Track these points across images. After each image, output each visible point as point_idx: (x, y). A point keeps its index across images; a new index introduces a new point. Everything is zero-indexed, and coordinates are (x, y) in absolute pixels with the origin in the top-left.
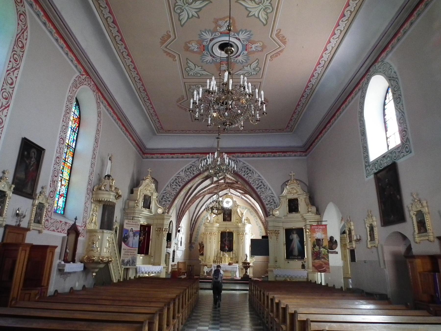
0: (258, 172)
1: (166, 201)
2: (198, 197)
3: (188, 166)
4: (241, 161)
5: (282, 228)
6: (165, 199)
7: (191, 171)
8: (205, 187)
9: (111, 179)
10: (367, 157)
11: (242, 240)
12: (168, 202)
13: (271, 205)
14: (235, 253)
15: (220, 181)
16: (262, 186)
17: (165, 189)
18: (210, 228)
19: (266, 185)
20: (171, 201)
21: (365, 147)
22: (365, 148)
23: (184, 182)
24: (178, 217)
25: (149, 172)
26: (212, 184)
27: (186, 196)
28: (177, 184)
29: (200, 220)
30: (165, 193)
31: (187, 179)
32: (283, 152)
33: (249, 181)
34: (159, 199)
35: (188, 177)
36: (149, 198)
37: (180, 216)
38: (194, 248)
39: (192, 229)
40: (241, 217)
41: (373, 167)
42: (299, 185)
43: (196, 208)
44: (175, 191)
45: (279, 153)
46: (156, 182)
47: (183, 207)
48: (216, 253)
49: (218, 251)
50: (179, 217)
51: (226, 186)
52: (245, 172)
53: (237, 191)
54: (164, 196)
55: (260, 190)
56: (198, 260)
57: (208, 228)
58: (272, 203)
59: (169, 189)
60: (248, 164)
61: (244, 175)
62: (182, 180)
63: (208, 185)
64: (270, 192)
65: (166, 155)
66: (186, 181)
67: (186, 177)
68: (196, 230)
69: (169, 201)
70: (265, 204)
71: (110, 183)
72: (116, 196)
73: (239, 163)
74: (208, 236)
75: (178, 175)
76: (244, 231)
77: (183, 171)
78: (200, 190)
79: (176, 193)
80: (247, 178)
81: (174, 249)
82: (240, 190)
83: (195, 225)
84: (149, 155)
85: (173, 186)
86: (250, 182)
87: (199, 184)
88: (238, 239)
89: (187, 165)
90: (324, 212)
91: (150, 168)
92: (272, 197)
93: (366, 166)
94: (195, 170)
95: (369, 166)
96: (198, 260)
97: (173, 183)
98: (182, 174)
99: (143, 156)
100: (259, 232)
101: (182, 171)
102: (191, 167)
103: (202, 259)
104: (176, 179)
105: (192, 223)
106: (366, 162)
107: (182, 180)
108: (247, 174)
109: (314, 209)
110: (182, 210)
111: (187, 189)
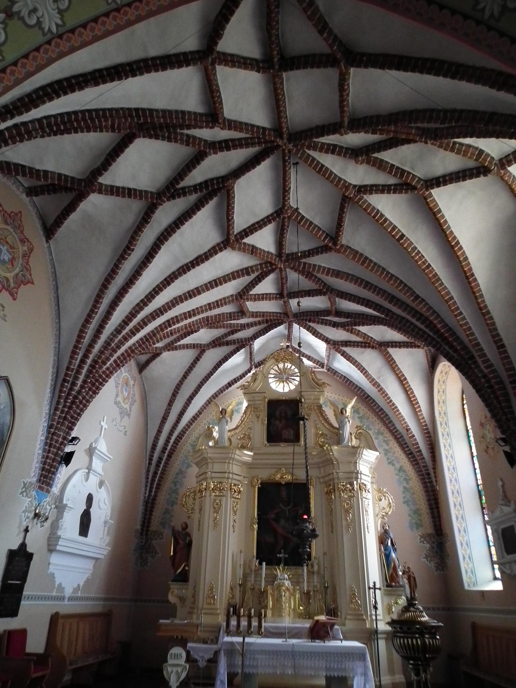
8: (196, 259)
11: (347, 511)
14: (318, 573)
18: (217, 467)
27: (105, 286)
29: (185, 447)
38: (156, 553)
39: (153, 480)
40: (336, 425)
43: (171, 403)
48: (240, 573)
49: (247, 565)
57: (210, 465)
63: (206, 249)
68: (167, 485)
74: (208, 498)
76: (355, 474)
78: (173, 273)
83: (165, 466)
87: (166, 230)
88: (331, 512)
100: (402, 489)
103: (182, 599)
105: (154, 462)
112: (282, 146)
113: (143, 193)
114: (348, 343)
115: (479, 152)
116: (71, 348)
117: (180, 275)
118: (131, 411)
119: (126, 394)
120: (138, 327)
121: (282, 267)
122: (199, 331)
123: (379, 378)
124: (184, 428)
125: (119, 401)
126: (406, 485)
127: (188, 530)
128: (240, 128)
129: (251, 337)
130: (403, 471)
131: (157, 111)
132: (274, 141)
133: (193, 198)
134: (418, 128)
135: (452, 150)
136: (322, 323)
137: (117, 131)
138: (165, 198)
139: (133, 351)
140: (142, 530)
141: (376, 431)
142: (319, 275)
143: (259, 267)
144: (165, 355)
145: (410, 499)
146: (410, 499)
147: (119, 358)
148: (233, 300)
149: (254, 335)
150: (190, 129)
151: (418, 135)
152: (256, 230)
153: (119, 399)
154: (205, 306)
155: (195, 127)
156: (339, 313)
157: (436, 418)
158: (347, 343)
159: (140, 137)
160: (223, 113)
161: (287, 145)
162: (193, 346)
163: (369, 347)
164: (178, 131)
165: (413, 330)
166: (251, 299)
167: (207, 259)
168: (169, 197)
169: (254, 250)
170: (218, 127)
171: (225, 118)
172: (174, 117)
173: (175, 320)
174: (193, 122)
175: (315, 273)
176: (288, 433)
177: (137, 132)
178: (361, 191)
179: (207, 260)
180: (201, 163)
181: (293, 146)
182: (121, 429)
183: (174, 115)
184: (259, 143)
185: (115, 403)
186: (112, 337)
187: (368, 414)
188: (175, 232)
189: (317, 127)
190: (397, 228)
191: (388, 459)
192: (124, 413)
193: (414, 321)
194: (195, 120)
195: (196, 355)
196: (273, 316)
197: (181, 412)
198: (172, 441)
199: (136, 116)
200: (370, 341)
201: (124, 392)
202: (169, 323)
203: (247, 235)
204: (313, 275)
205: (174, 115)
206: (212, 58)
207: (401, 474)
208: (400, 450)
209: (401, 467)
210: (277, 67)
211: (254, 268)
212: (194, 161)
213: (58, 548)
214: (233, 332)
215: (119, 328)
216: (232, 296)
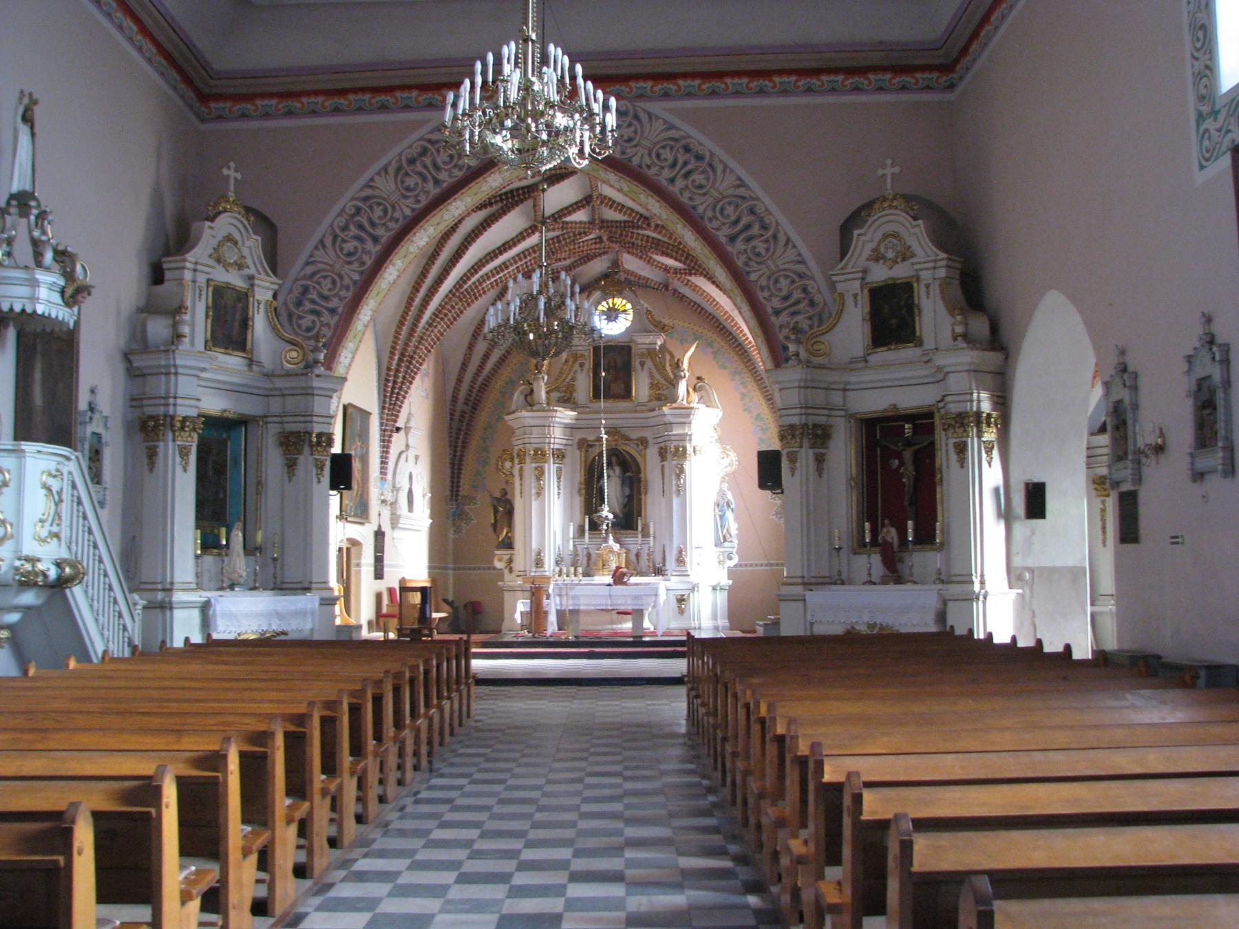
0: (732, 164)
1: (317, 313)
2: (474, 294)
3: (410, 147)
4: (657, 118)
5: (842, 413)
6: (313, 301)
7: (425, 172)
8: (503, 245)
9: (35, 212)
10: (1208, 72)
12: (326, 317)
13: (793, 314)
15: (570, 213)
16: (756, 230)
17: (311, 256)
19: (774, 225)
20: (340, 310)
21: (1203, 27)
22: (1201, 34)
23: (397, 220)
24: (386, 385)
25: (232, 181)
26: (533, 229)
28: (363, 234)
30: (313, 274)
31: (407, 210)
32: (850, 71)
33: (694, 208)
34: (285, 303)
35: (411, 200)
36: (239, 300)
37: (395, 382)
41: (1232, 120)
42: (920, 222)
43: (471, 347)
44: (355, 266)
45: (832, 78)
46: (264, 224)
47: (409, 338)
50: (393, 388)
51: (600, 238)
52: (674, 165)
53: (649, 261)
54: (306, 290)
55: (743, 247)
56: (489, 568)
58: (801, 306)
59: (327, 257)
60: (686, 128)
61: (672, 181)
62: (386, 211)
64: (791, 254)
65: (305, 100)
66: (405, 217)
67: (406, 197)
69: (333, 311)
70: (770, 310)
71: (30, 231)
72: (64, 287)
73: (647, 126)
75: (368, 192)
77: (386, 172)
79: (361, 273)
80: (687, 194)
81: (380, 526)
82: (665, 254)
84: (229, 104)
85: (344, 241)
86: (700, 209)
89: (405, 144)
90: (1022, 336)
91: (232, 165)
92: (801, 276)
93: (1201, 117)
94: (444, 163)
95: (1214, 113)
96: (489, 568)
97: (345, 228)
98: (386, 186)
99: (203, 109)
101: (385, 169)
102: (424, 152)
104: (358, 211)
106: (1202, 98)
107: (386, 211)
108: (687, 175)
109: (980, 326)
110: (402, 355)
111: (410, 257)
116: (388, 349)
127: (508, 497)
140: (452, 495)
176: (617, 388)
197: (484, 355)
209: (759, 414)
213: (400, 525)
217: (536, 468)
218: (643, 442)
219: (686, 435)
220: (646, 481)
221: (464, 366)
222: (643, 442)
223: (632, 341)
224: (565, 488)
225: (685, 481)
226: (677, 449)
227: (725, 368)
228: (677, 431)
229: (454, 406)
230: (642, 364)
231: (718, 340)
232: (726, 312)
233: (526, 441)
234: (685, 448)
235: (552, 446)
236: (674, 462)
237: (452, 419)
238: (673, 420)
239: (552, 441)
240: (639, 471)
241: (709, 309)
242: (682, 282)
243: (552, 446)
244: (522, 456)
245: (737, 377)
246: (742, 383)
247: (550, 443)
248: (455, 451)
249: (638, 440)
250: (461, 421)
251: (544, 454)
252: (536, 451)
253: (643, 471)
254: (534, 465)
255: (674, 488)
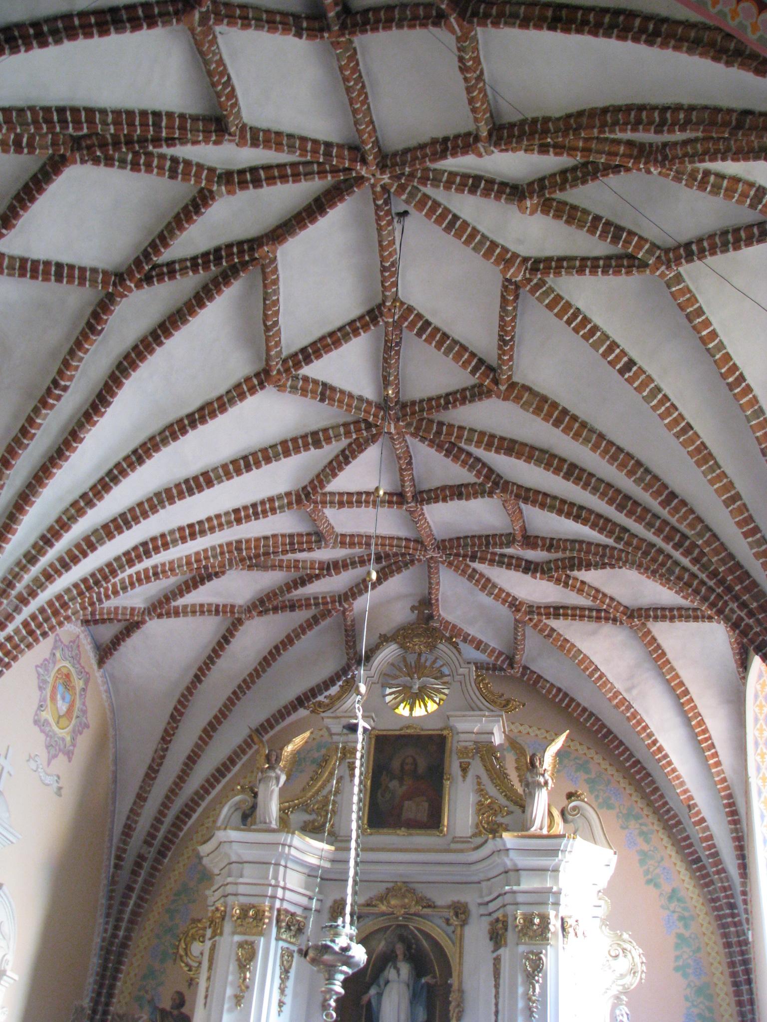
8: (201, 409)
43: (167, 737)
112: (369, 179)
113: (88, 273)
114: (561, 611)
115: (757, 190)
117: (165, 442)
118: (74, 745)
119: (63, 707)
120: (77, 553)
121: (393, 430)
122: (223, 573)
123: (629, 690)
124: (197, 793)
125: (46, 721)
126: (682, 931)
127: (184, 1010)
128: (276, 144)
129: (346, 594)
130: (678, 900)
131: (103, 112)
132: (350, 169)
133: (187, 284)
134: (630, 143)
135: (702, 186)
136: (501, 563)
137: (26, 151)
138: (131, 281)
139: (64, 605)
141: (625, 812)
142: (480, 452)
143: (342, 430)
144: (154, 627)
145: (689, 961)
146: (689, 961)
147: (34, 617)
148: (290, 504)
149: (351, 589)
150: (174, 145)
151: (630, 156)
152: (327, 349)
153: (46, 715)
154: (227, 514)
155: (183, 141)
156: (530, 541)
157: (750, 780)
158: (558, 611)
159: (75, 162)
160: (238, 115)
161: (378, 176)
162: (217, 610)
163: (607, 619)
164: (151, 148)
165: (670, 571)
166: (332, 503)
167: (223, 408)
168: (141, 280)
169: (328, 392)
170: (230, 141)
171: (244, 126)
172: (137, 123)
173: (160, 543)
174: (177, 131)
175: (462, 445)
176: (415, 809)
177: (68, 154)
178: (538, 270)
179: (222, 412)
180: (327, 213)
181: (389, 178)
182: (48, 780)
183: (137, 119)
184: (322, 173)
185: (36, 722)
186: (17, 569)
187: (609, 772)
188: (151, 351)
189: (434, 142)
190: (618, 347)
191: (647, 872)
192: (55, 748)
193: (668, 548)
194: (182, 128)
195: (223, 631)
196: (391, 546)
197: (189, 758)
198: (168, 820)
199: (59, 122)
200: (609, 605)
201: (60, 702)
202: (146, 549)
203: (308, 360)
204: (461, 450)
205: (137, 119)
206: (201, 13)
207: (672, 906)
208: (673, 854)
209: (673, 891)
210: (337, 28)
211: (331, 432)
212: (191, 208)
214: (303, 582)
215: (33, 552)
216: (288, 494)
217: (241, 945)
218: (460, 911)
219: (549, 891)
220: (461, 991)
221: (152, 772)
222: (460, 911)
223: (451, 728)
224: (295, 995)
225: (544, 987)
226: (528, 920)
227: (610, 807)
228: (528, 884)
229: (125, 843)
230: (464, 769)
231: (598, 758)
232: (617, 693)
233: (230, 889)
234: (545, 920)
235: (278, 904)
236: (522, 949)
237: (117, 867)
238: (523, 861)
239: (280, 893)
240: (447, 970)
241: (585, 695)
242: (542, 631)
243: (278, 904)
244: (216, 924)
245: (633, 824)
246: (642, 833)
247: (274, 897)
248: (116, 928)
249: (449, 907)
250: (134, 873)
251: (259, 916)
252: (244, 910)
253: (455, 974)
254: (237, 938)
255: (521, 1004)
